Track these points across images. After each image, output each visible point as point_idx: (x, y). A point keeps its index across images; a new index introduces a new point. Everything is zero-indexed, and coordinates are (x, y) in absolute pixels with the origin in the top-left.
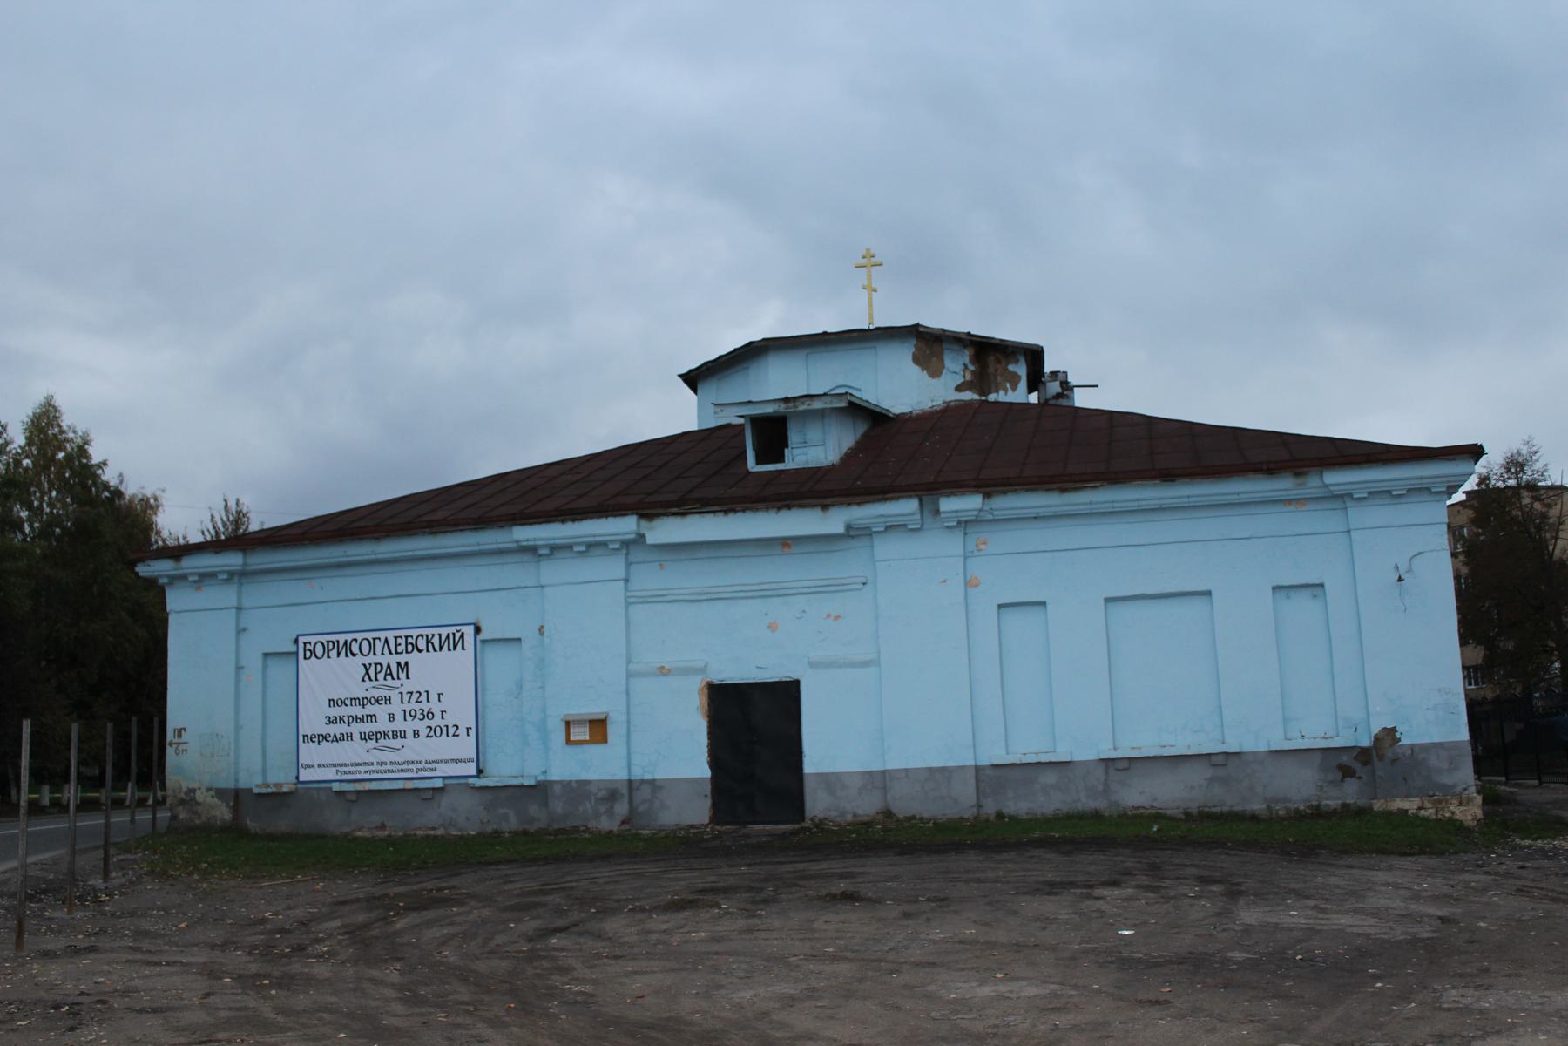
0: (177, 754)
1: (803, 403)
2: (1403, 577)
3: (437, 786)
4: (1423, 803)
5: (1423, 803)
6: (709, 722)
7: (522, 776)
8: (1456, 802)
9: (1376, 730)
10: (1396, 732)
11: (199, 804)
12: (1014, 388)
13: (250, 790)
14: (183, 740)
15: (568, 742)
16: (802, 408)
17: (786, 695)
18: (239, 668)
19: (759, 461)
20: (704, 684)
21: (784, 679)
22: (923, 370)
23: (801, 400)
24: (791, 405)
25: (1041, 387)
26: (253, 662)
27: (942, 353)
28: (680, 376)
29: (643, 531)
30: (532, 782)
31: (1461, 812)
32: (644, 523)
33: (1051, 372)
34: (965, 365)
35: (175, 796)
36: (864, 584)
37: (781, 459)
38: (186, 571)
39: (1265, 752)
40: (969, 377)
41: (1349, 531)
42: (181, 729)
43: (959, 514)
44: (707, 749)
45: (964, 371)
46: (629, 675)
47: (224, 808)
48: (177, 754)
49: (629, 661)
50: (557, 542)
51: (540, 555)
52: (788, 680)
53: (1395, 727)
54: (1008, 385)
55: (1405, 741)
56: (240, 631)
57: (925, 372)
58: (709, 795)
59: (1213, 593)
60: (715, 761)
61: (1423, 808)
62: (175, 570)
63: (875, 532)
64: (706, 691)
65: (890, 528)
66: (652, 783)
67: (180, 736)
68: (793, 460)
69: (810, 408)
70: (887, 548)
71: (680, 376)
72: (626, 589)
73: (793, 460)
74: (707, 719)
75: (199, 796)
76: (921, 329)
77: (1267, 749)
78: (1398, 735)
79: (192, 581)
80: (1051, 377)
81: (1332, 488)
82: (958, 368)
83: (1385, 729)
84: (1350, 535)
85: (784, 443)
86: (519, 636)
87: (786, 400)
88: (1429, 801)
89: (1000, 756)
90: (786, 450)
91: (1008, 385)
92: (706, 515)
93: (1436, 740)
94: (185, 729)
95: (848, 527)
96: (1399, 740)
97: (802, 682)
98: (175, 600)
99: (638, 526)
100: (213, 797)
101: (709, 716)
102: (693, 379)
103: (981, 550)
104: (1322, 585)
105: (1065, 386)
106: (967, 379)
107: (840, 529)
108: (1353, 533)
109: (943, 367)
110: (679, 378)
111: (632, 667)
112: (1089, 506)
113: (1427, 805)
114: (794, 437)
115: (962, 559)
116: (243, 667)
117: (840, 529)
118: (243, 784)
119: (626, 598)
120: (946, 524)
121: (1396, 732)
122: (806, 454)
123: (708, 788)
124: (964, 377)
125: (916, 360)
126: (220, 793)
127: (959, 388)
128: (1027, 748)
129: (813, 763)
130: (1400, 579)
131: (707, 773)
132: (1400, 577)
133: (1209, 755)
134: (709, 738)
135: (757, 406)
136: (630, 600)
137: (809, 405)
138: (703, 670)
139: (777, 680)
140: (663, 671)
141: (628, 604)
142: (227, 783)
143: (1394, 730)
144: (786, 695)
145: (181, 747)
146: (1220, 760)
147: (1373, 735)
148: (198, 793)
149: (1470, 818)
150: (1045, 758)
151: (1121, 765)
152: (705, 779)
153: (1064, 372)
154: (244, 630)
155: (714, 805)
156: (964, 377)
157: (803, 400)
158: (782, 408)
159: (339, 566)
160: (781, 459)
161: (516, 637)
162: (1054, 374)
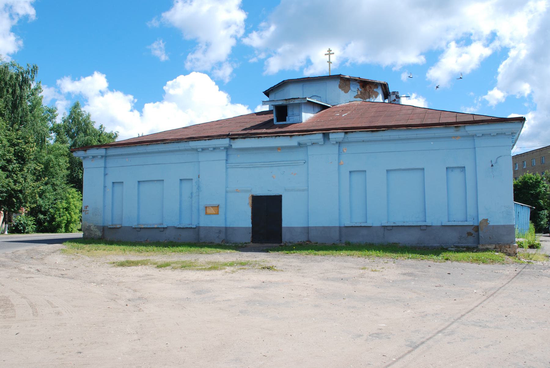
0: (85, 214)
1: (292, 101)
2: (493, 165)
3: (165, 227)
4: (496, 247)
5: (496, 247)
6: (252, 208)
7: (192, 224)
8: (508, 246)
9: (480, 219)
10: (488, 220)
11: (92, 230)
12: (376, 97)
13: (107, 226)
14: (87, 210)
15: (206, 213)
16: (291, 102)
17: (276, 201)
18: (105, 187)
19: (278, 121)
20: (250, 195)
21: (277, 195)
22: (342, 91)
23: (291, 100)
24: (288, 101)
25: (389, 97)
26: (109, 185)
27: (350, 84)
28: (263, 92)
29: (231, 144)
30: (195, 227)
31: (510, 250)
32: (232, 141)
33: (393, 92)
34: (358, 89)
35: (85, 228)
36: (304, 163)
37: (285, 121)
38: (88, 155)
39: (440, 226)
40: (359, 93)
41: (475, 148)
42: (87, 206)
43: (336, 139)
44: (251, 217)
45: (357, 91)
46: (227, 192)
47: (99, 232)
48: (85, 214)
49: (227, 187)
50: (217, 146)
51: (199, 151)
52: (278, 195)
53: (487, 219)
54: (374, 96)
55: (491, 224)
56: (105, 175)
57: (343, 91)
58: (251, 233)
59: (367, 171)
60: (253, 222)
61: (496, 248)
62: (85, 154)
63: (308, 145)
64: (251, 198)
65: (313, 144)
66: (233, 228)
67: (86, 208)
68: (289, 120)
69: (294, 102)
70: (312, 151)
71: (263, 92)
72: (227, 163)
73: (289, 120)
74: (251, 207)
75: (92, 228)
76: (341, 76)
77: (441, 225)
78: (488, 222)
79: (99, 158)
80: (393, 94)
81: (468, 132)
82: (356, 90)
83: (484, 219)
84: (475, 149)
85: (286, 115)
86: (123, 181)
87: (286, 100)
88: (498, 246)
89: (347, 223)
90: (287, 117)
91: (374, 96)
92: (252, 138)
93: (502, 224)
94: (88, 206)
95: (299, 144)
96: (489, 223)
97: (282, 196)
98: (86, 164)
99: (230, 142)
100: (96, 228)
101: (252, 206)
102: (267, 93)
103: (344, 152)
104: (465, 167)
105: (397, 97)
106: (358, 94)
107: (296, 144)
108: (476, 148)
109: (350, 89)
110: (263, 93)
111: (228, 189)
112: (381, 137)
113: (497, 247)
114: (290, 112)
115: (337, 155)
116: (106, 187)
117: (296, 144)
118: (105, 225)
119: (226, 166)
120: (332, 143)
121: (488, 220)
122: (293, 119)
123: (251, 231)
124: (358, 93)
125: (340, 87)
126: (98, 227)
127: (355, 97)
128: (358, 221)
129: (285, 223)
130: (492, 166)
131: (251, 226)
132: (492, 165)
133: (421, 226)
134: (252, 214)
135: (277, 102)
136: (228, 167)
137: (294, 101)
138: (250, 191)
139: (275, 195)
140: (237, 191)
141: (227, 168)
142: (101, 224)
143: (487, 220)
144: (276, 201)
145: (87, 212)
146: (425, 228)
147: (479, 222)
148: (92, 227)
149: (513, 252)
150: (363, 225)
151: (389, 228)
152: (250, 227)
153: (397, 92)
154: (107, 174)
155: (253, 236)
156: (358, 93)
157: (292, 100)
158: (285, 103)
159: (122, 155)
160: (285, 121)
161: (421, 167)
162: (394, 93)
